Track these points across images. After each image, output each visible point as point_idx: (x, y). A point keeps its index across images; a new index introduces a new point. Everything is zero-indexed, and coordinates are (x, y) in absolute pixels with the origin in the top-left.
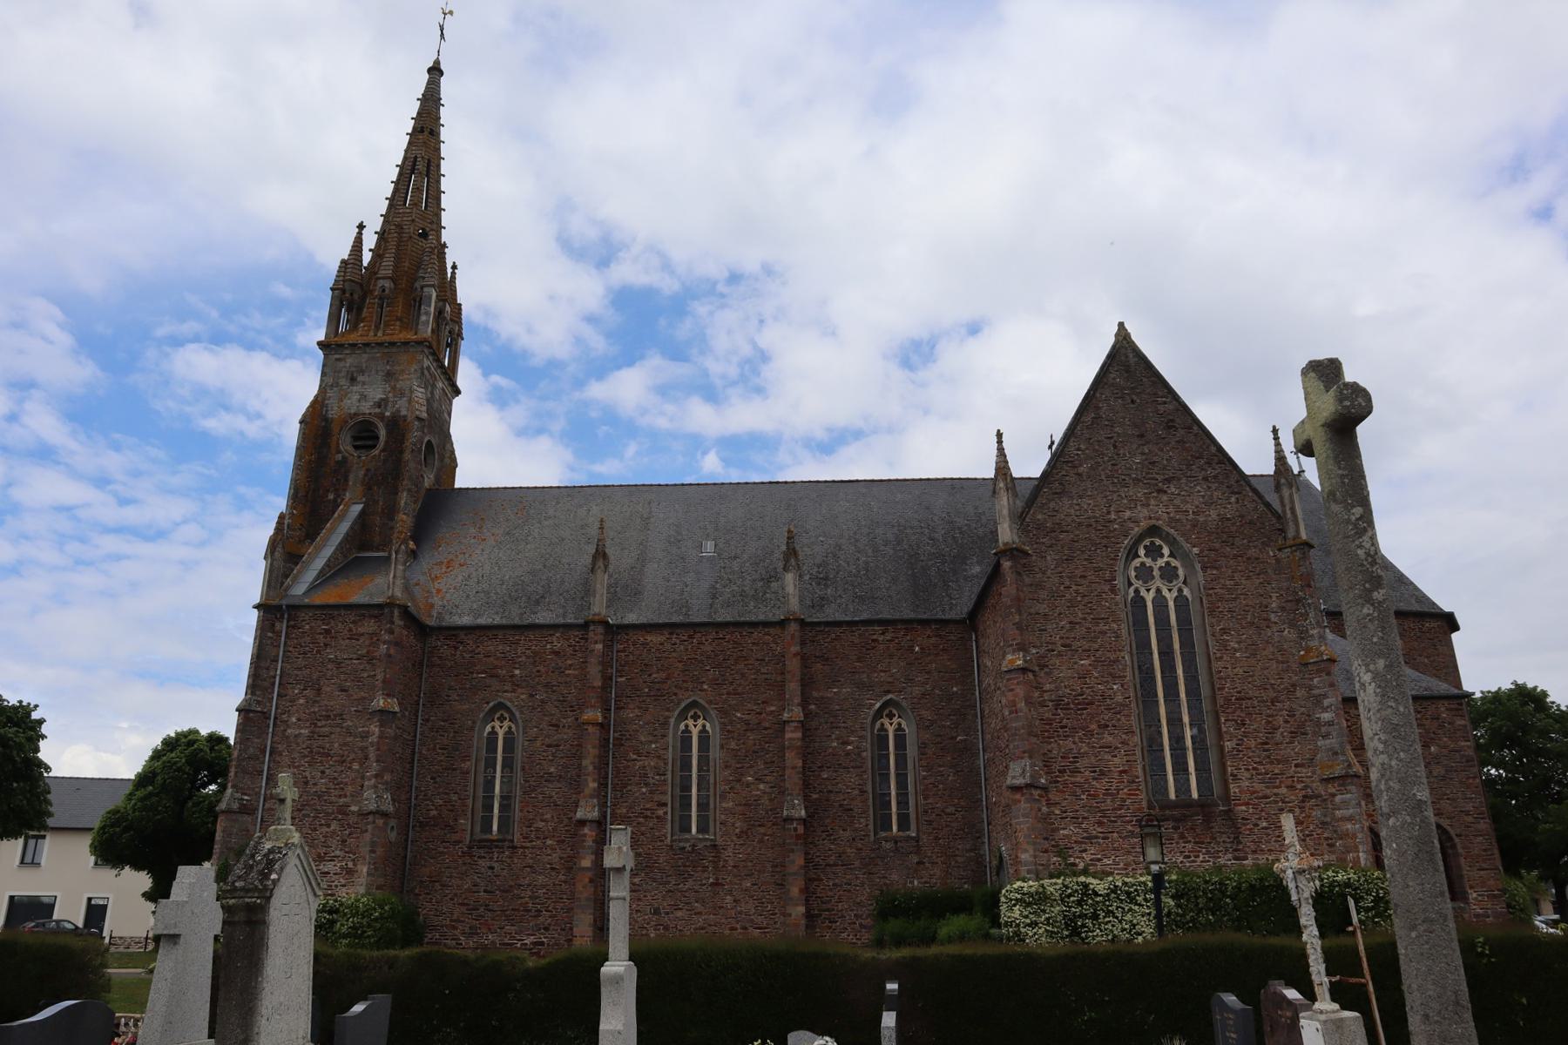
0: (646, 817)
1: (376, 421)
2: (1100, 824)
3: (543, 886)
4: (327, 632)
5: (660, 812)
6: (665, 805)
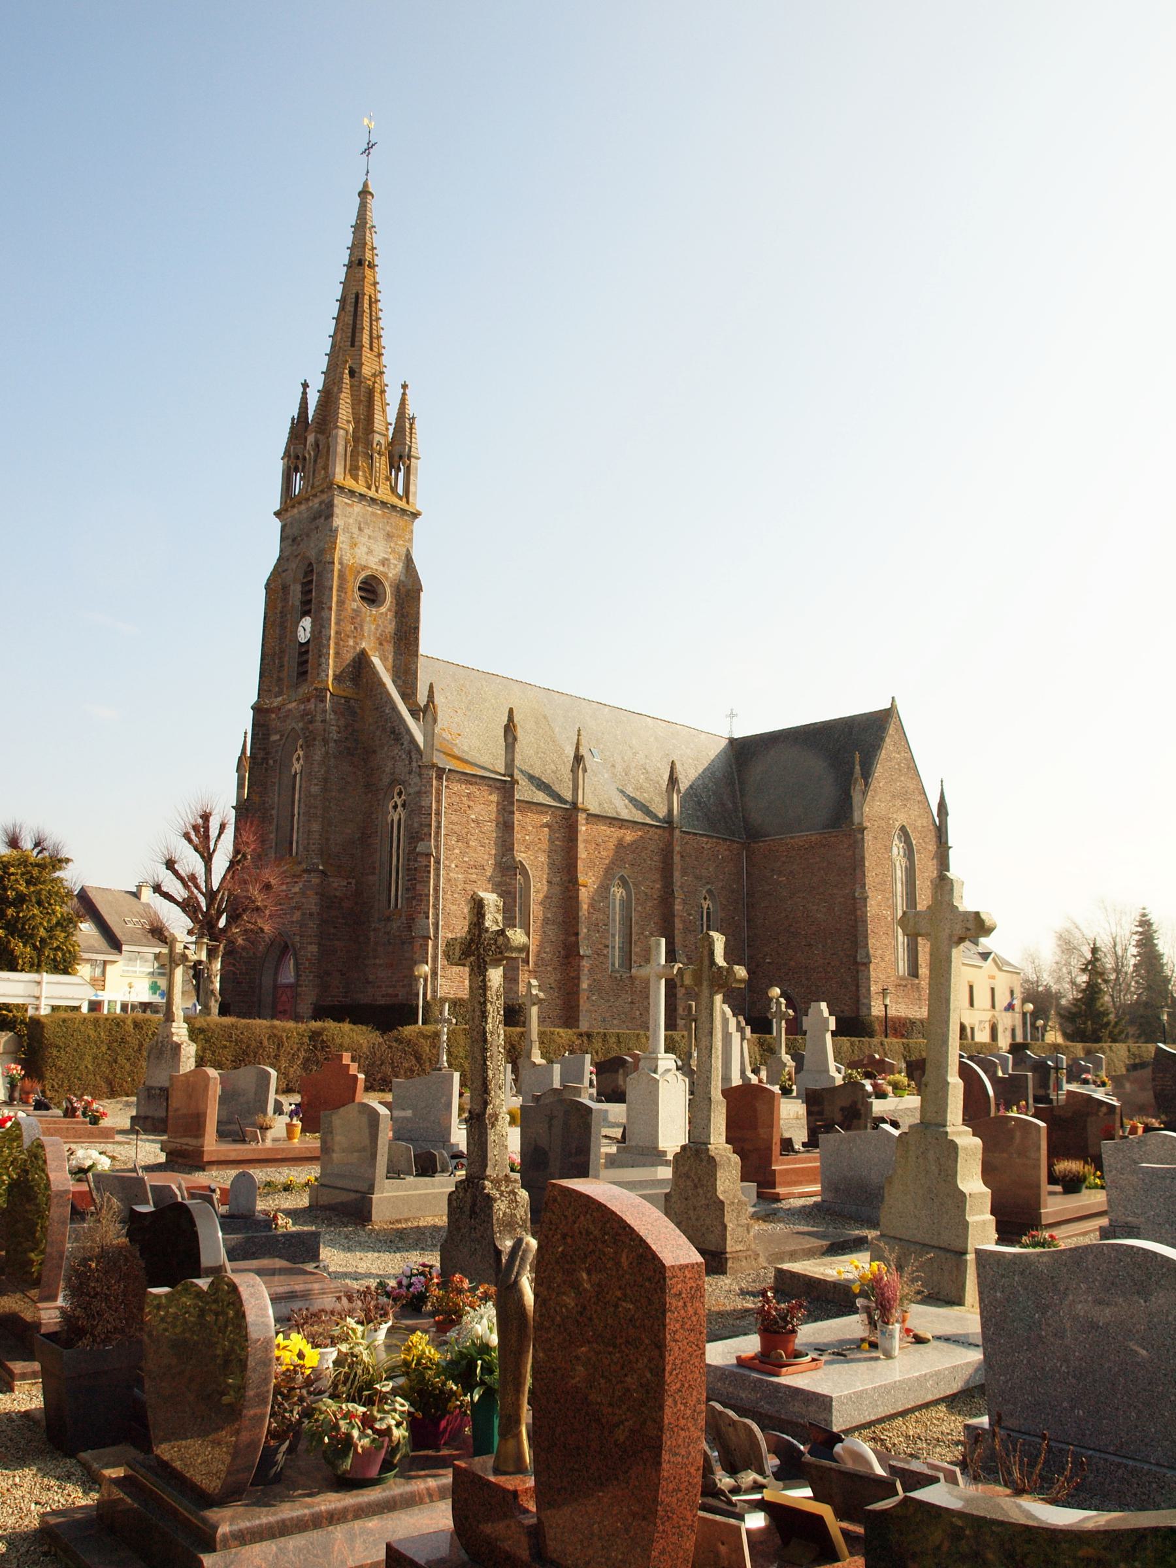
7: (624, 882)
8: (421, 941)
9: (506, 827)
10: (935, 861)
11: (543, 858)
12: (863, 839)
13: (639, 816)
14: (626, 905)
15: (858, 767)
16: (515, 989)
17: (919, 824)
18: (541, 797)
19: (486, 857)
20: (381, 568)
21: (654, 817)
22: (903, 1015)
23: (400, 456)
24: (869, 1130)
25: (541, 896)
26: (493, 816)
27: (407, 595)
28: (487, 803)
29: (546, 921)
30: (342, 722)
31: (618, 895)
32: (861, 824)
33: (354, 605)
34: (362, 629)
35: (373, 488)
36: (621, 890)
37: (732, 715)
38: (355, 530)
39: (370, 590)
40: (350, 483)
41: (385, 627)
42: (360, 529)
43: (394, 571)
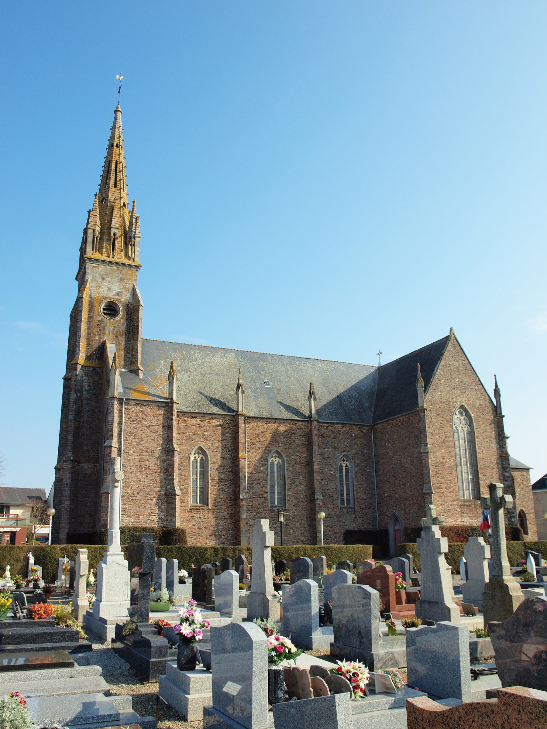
0: (260, 497)
1: (117, 302)
2: (448, 506)
3: (222, 526)
4: (143, 412)
5: (265, 496)
6: (267, 492)
7: (279, 455)
8: (105, 495)
9: (168, 428)
10: (493, 426)
11: (217, 444)
12: (424, 416)
13: (288, 415)
14: (281, 468)
15: (419, 372)
16: (173, 520)
17: (477, 403)
18: (216, 410)
19: (155, 446)
20: (117, 297)
21: (303, 415)
22: (468, 524)
23: (129, 239)
24: (404, 604)
25: (216, 466)
26: (161, 422)
27: (133, 309)
28: (156, 415)
29: (220, 480)
30: (91, 380)
31: (276, 463)
32: (423, 407)
33: (99, 318)
34: (104, 329)
35: (111, 256)
36: (277, 459)
37: (379, 353)
38: (100, 280)
39: (111, 309)
40: (98, 256)
41: (119, 327)
42: (103, 279)
43: (126, 297)
